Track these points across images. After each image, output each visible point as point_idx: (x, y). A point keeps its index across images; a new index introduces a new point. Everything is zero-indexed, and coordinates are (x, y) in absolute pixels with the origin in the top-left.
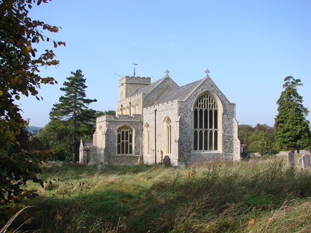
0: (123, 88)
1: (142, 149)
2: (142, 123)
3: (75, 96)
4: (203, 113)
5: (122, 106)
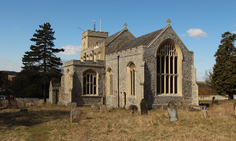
0: (86, 40)
2: (105, 68)
3: (45, 46)
4: (161, 59)
5: (85, 54)
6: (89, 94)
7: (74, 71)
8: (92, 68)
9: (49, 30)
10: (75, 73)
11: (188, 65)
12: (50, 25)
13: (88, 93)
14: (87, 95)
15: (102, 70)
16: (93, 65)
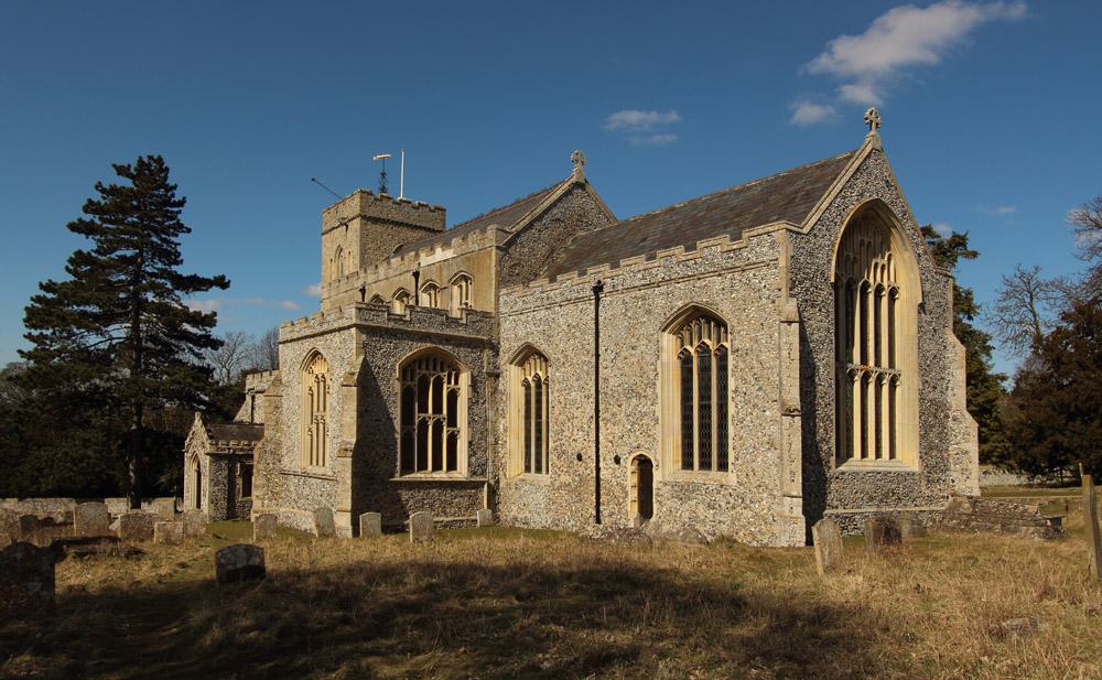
1: (496, 452)
5: (363, 291)
6: (426, 468)
7: (362, 358)
8: (441, 347)
9: (162, 191)
10: (365, 365)
11: (935, 331)
12: (167, 169)
13: (423, 467)
14: (419, 475)
15: (485, 358)
16: (448, 332)
